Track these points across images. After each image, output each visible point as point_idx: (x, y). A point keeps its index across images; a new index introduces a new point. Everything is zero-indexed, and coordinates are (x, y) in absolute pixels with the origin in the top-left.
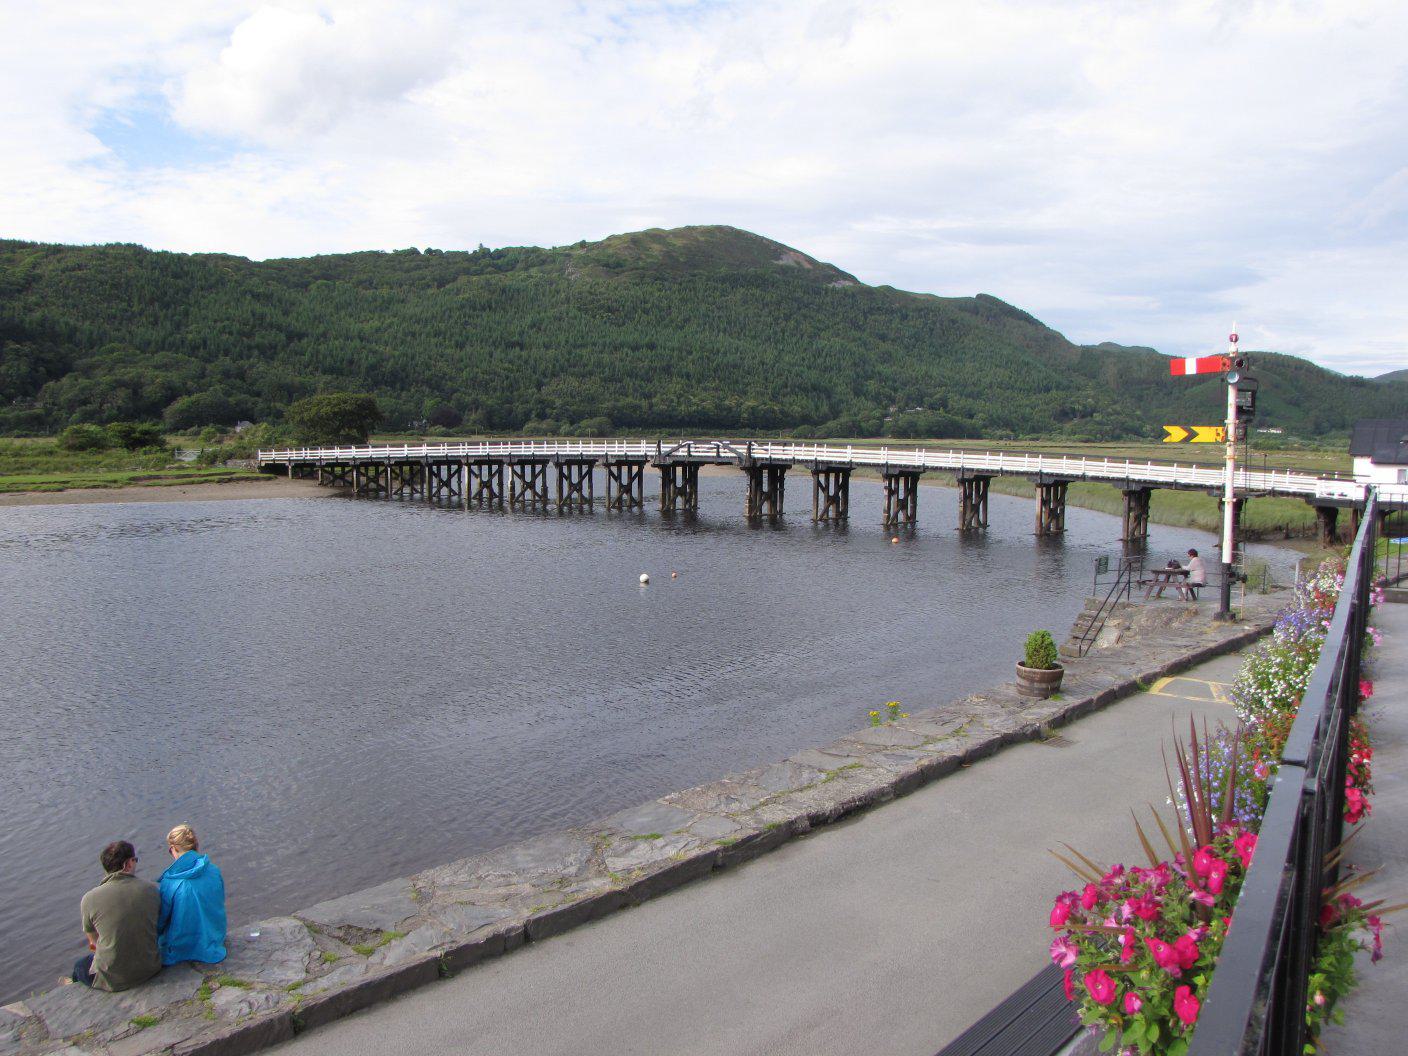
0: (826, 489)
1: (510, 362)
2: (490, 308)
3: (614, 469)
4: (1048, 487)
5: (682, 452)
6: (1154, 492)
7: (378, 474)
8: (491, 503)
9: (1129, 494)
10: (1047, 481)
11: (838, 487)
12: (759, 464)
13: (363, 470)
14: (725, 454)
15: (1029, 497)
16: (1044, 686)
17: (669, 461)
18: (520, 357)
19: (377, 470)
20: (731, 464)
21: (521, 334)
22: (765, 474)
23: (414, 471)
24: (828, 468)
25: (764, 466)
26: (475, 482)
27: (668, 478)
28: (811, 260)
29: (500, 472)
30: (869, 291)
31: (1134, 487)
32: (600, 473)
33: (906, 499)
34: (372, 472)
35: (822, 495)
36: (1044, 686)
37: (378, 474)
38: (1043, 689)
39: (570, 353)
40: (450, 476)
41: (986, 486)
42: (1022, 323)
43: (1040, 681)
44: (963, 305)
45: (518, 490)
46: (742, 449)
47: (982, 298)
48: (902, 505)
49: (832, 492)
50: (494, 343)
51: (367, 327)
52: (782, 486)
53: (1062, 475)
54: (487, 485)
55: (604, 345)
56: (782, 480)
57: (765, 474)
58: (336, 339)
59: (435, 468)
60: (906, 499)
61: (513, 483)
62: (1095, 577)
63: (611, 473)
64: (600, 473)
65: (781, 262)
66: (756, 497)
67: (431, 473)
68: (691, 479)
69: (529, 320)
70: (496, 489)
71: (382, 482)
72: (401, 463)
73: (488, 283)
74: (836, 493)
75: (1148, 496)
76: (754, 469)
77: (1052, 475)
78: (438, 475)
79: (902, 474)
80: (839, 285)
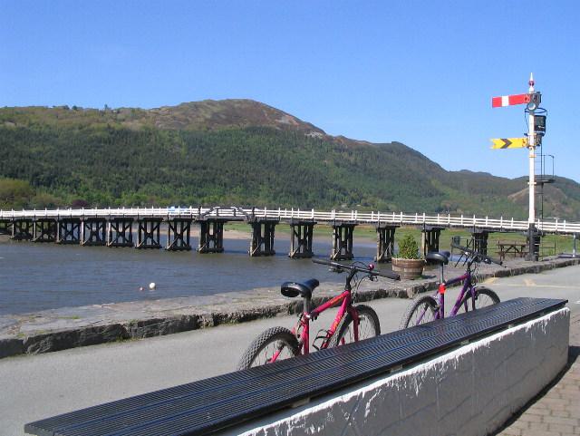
0: (299, 236)
1: (121, 174)
2: (110, 142)
3: (173, 225)
4: (429, 232)
5: (213, 214)
6: (490, 235)
7: (28, 227)
8: (97, 242)
9: (476, 235)
10: (428, 228)
11: (346, 237)
12: (258, 220)
13: (18, 224)
14: (239, 214)
15: (552, 180)
16: (411, 271)
17: (205, 219)
18: (126, 171)
19: (28, 224)
20: (242, 220)
21: (127, 158)
22: (263, 226)
23: (50, 226)
24: (300, 223)
25: (262, 222)
26: (88, 232)
27: (205, 230)
28: (298, 120)
29: (104, 227)
30: (330, 139)
31: (478, 231)
32: (164, 230)
33: (345, 242)
34: (24, 226)
35: (296, 239)
36: (411, 271)
37: (28, 227)
38: (410, 273)
39: (156, 169)
40: (73, 229)
41: (393, 232)
42: (416, 158)
43: (408, 268)
44: (383, 147)
45: (114, 237)
46: (249, 212)
47: (398, 150)
48: (343, 244)
49: (302, 237)
50: (110, 163)
51: (34, 150)
52: (273, 234)
53: (437, 225)
54: (96, 234)
55: (177, 166)
56: (273, 230)
57: (263, 226)
58: (15, 156)
59: (18, 224)
60: (345, 242)
61: (111, 232)
62: (569, 425)
63: (170, 226)
64: (164, 230)
65: (280, 121)
66: (257, 239)
67: (61, 226)
68: (219, 231)
69: (132, 150)
70: (101, 237)
71: (30, 232)
72: (43, 220)
73: (109, 127)
74: (346, 240)
75: (487, 237)
76: (256, 224)
77: (431, 225)
78: (65, 228)
79: (343, 225)
80: (314, 135)
